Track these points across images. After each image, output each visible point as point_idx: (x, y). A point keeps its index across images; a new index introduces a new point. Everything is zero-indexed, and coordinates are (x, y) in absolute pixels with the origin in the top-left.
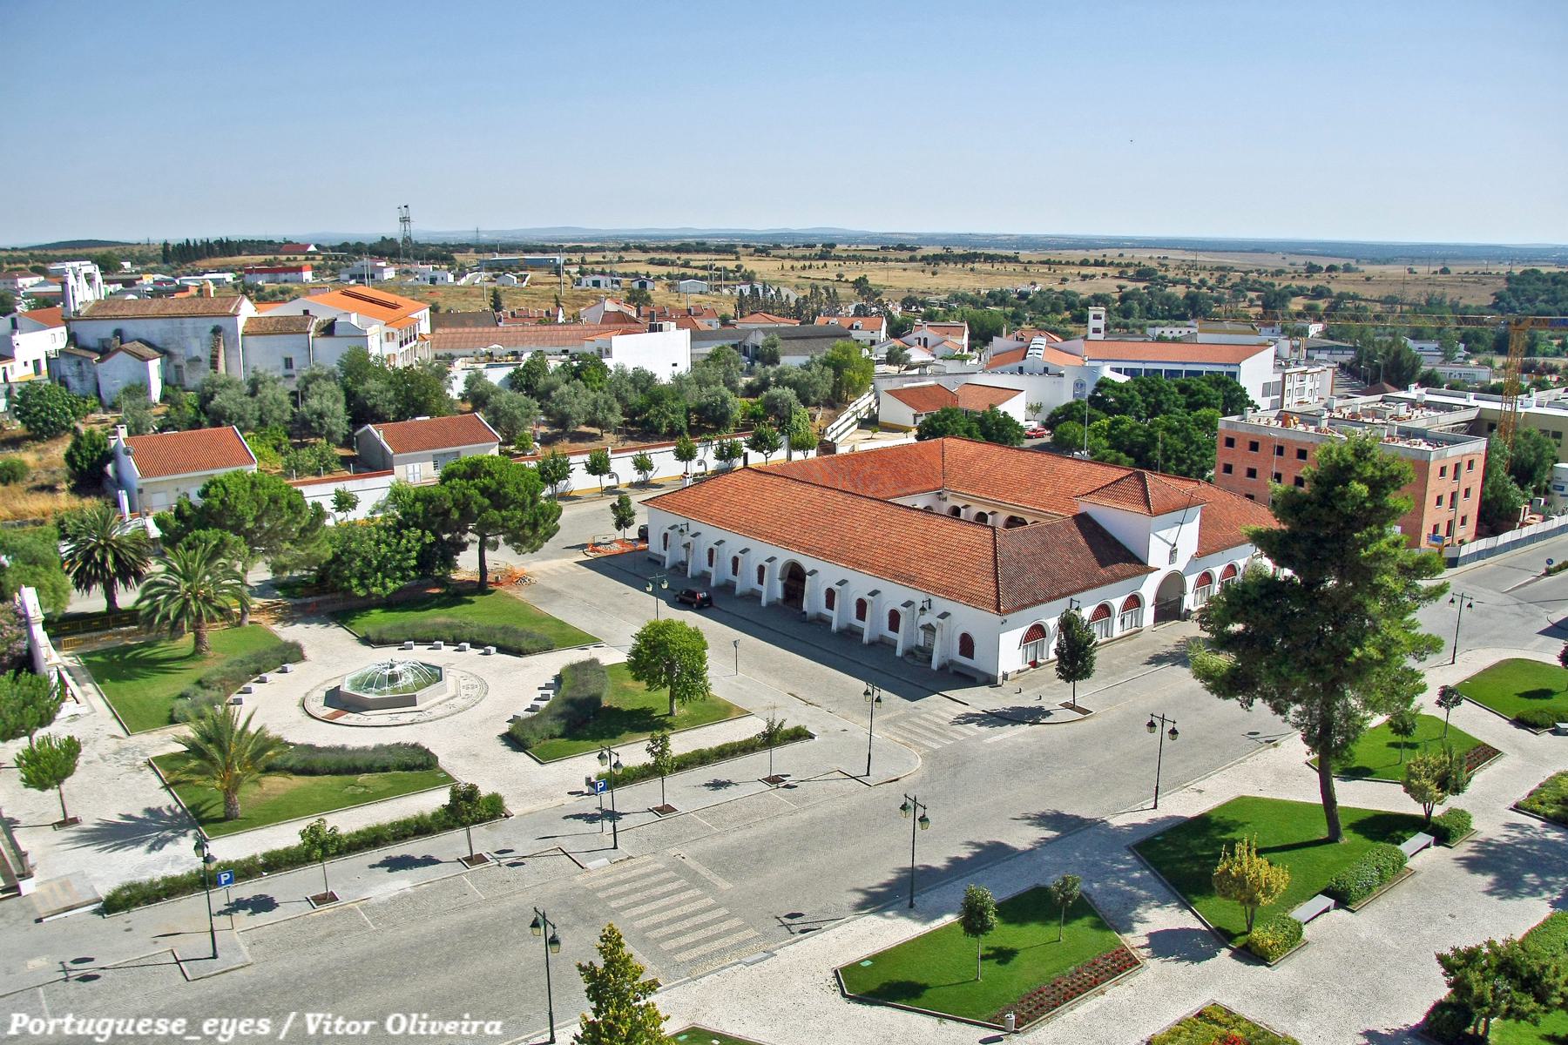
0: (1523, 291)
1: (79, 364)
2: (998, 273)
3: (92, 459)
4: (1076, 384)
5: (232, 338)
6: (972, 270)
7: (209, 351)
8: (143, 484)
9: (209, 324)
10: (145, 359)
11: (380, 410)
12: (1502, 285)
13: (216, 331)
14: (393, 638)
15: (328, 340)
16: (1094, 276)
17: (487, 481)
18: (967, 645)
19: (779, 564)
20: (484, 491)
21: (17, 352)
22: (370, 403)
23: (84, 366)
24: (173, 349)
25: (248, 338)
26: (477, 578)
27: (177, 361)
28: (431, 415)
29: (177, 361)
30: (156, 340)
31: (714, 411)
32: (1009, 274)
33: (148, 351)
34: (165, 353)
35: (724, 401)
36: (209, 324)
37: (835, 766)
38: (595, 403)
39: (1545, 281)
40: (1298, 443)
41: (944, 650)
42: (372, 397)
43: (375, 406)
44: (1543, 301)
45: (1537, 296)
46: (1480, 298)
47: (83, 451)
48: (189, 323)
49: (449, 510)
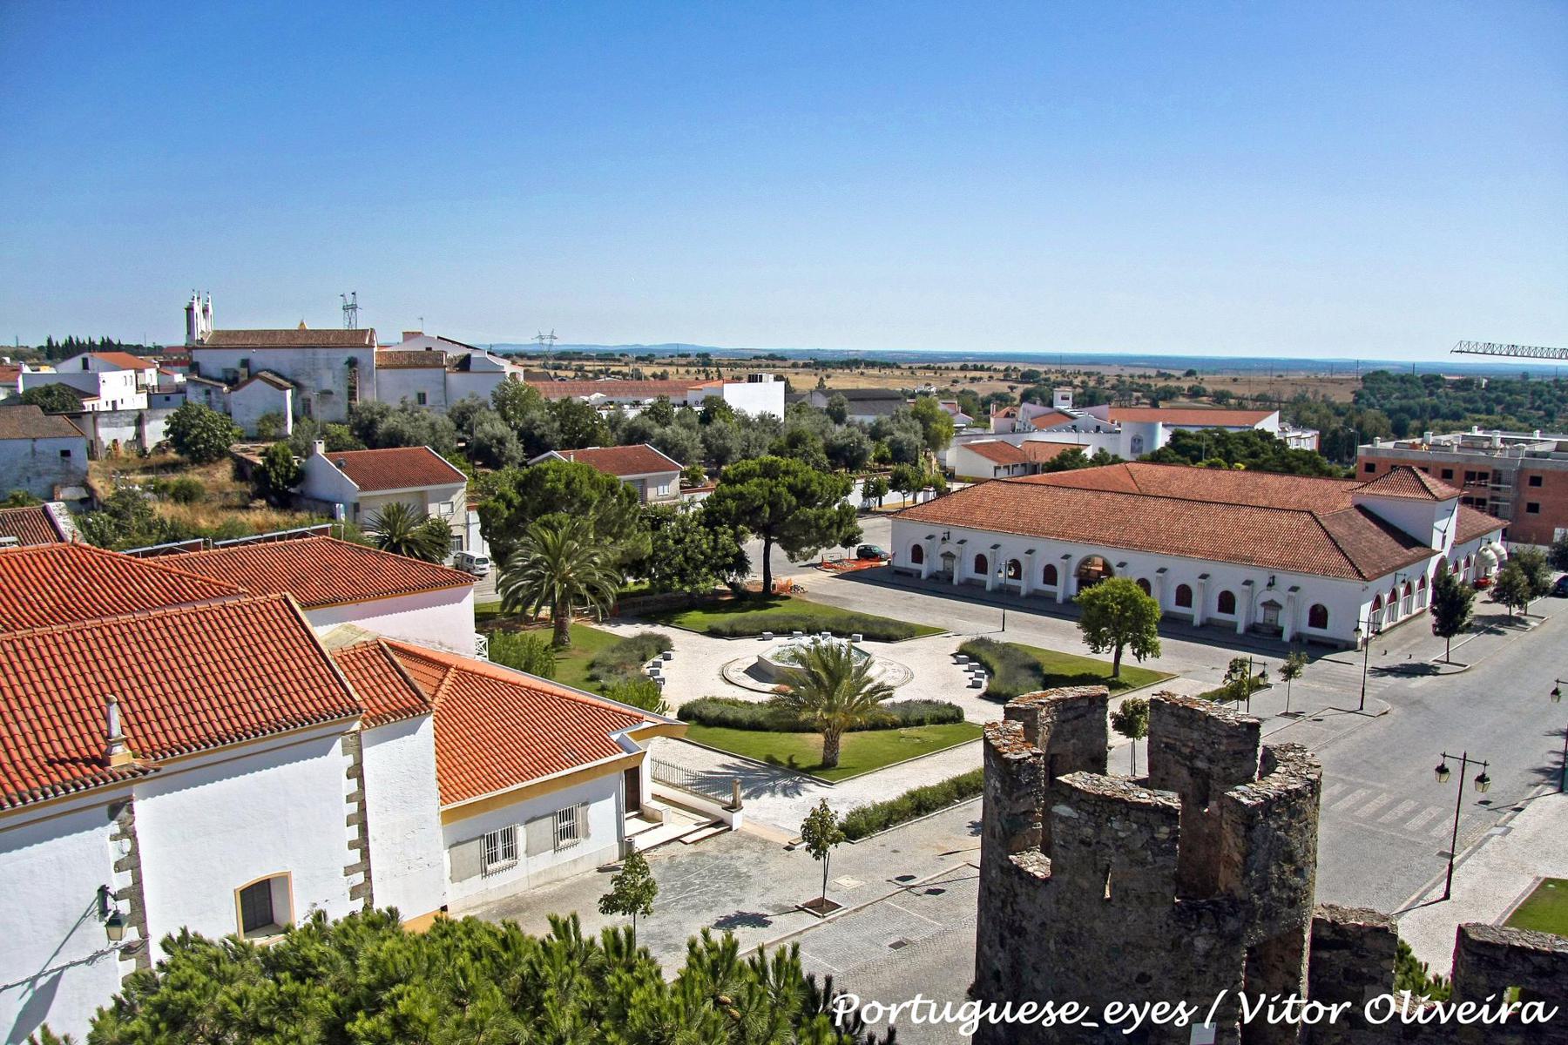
0: (1379, 389)
1: (208, 393)
2: (886, 377)
3: (287, 476)
4: (1134, 440)
5: (368, 369)
6: (862, 374)
7: (347, 383)
8: (361, 498)
9: (345, 355)
10: (283, 388)
11: (548, 440)
12: (1359, 386)
13: (352, 363)
14: (747, 630)
15: (463, 376)
16: (981, 378)
17: (790, 479)
18: (1318, 616)
19: (1074, 563)
20: (791, 488)
21: (103, 390)
22: (537, 432)
23: (213, 395)
24: (303, 381)
25: (382, 371)
26: (760, 588)
27: (306, 394)
28: (601, 445)
29: (306, 394)
30: (286, 371)
31: (851, 452)
32: (898, 378)
33: (287, 384)
34: (298, 386)
35: (860, 443)
36: (345, 355)
37: (1326, 704)
38: (748, 440)
39: (1395, 381)
40: (1442, 464)
41: (1292, 622)
42: (539, 427)
43: (543, 436)
44: (1397, 398)
45: (1391, 394)
46: (1343, 397)
47: (278, 467)
48: (322, 353)
49: (760, 508)
